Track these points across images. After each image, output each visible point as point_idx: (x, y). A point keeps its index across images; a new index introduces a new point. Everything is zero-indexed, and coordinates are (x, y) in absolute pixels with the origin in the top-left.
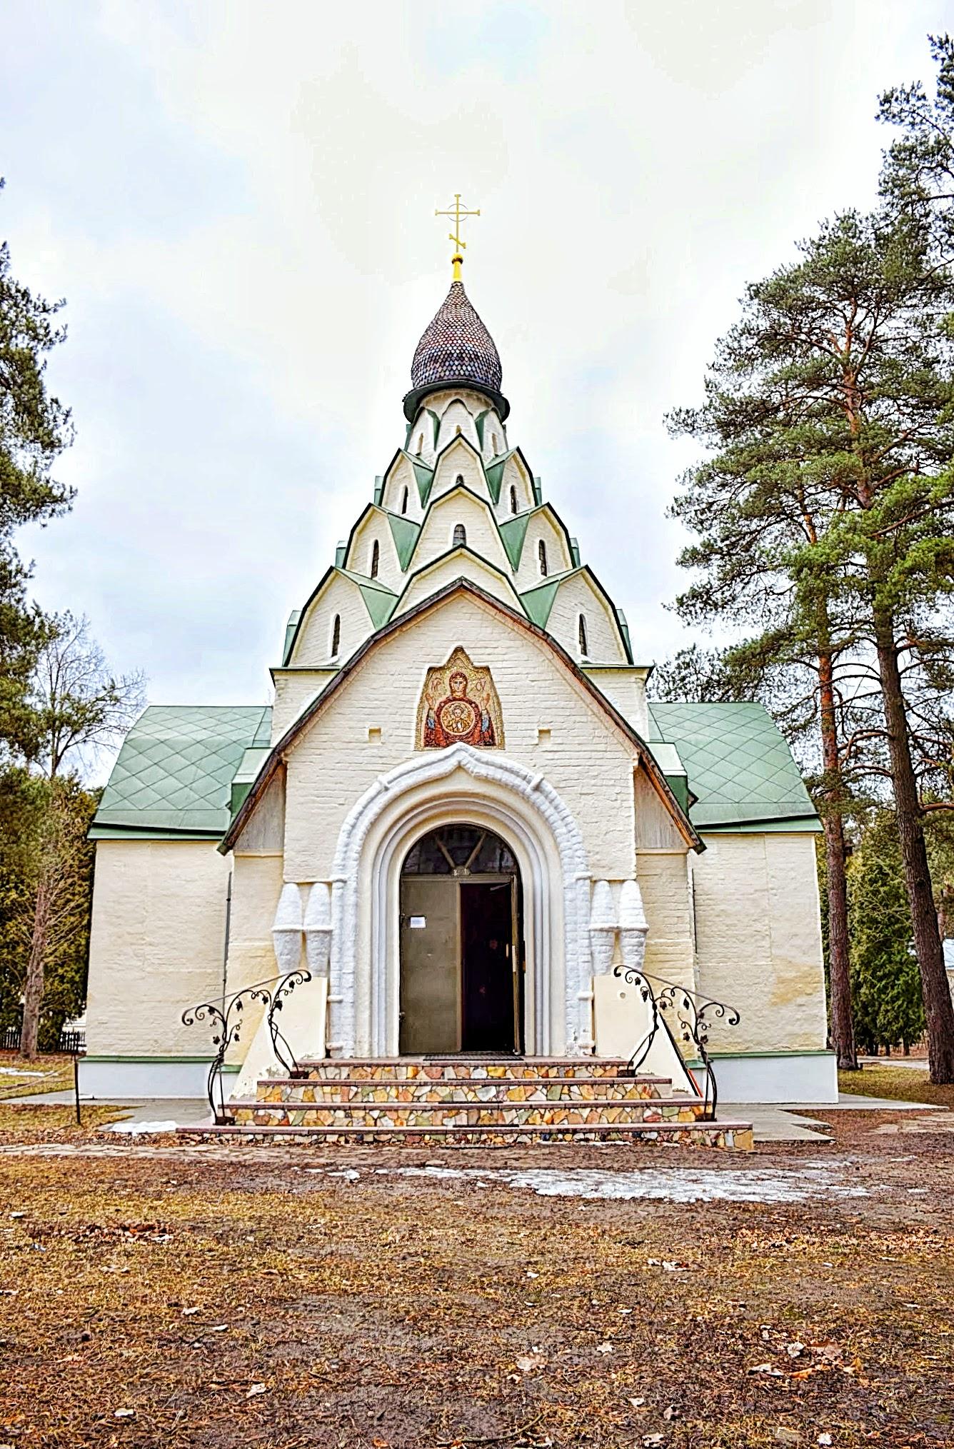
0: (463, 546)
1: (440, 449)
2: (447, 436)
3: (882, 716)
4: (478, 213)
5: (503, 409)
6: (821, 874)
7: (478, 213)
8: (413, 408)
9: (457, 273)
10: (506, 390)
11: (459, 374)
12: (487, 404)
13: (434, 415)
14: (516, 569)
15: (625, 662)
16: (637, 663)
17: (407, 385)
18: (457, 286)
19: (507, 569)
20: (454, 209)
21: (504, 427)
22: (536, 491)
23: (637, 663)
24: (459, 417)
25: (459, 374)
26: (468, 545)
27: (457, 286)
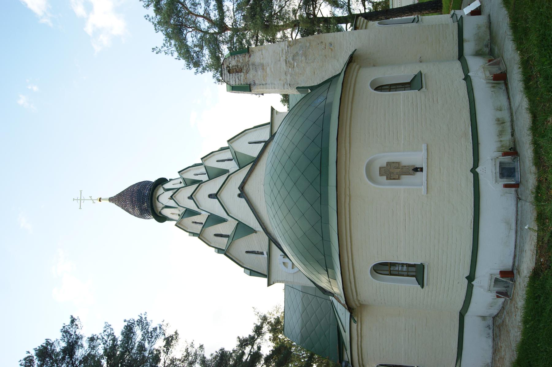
0: (216, 194)
1: (177, 206)
2: (172, 203)
3: (286, 32)
5: (162, 181)
8: (161, 218)
9: (105, 199)
10: (153, 179)
11: (143, 199)
13: (163, 208)
14: (228, 171)
16: (199, 233)
17: (153, 221)
18: (111, 200)
21: (171, 180)
22: (196, 165)
23: (199, 233)
24: (164, 198)
25: (143, 199)
26: (215, 192)
27: (111, 200)
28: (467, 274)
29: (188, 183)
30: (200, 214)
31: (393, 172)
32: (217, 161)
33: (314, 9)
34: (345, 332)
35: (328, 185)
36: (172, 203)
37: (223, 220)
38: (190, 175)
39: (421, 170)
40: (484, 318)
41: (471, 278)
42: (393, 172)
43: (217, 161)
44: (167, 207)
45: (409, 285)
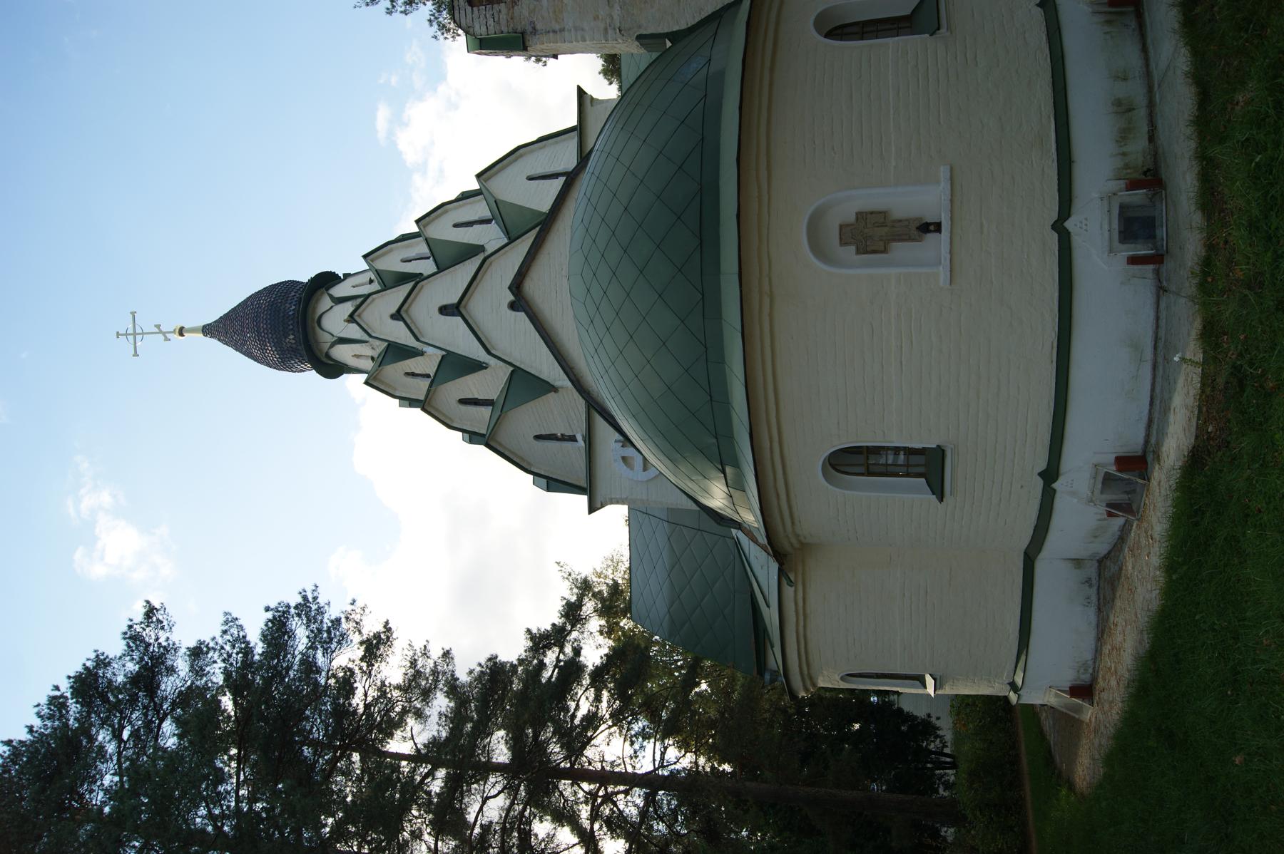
1: (366, 337)
2: (353, 331)
4: (136, 355)
5: (326, 280)
6: (952, 706)
7: (136, 355)
8: (332, 369)
9: (193, 330)
10: (304, 277)
12: (328, 356)
13: (333, 345)
14: (481, 249)
15: (575, 134)
18: (208, 330)
19: (481, 257)
20: (131, 338)
21: (347, 276)
27: (208, 330)
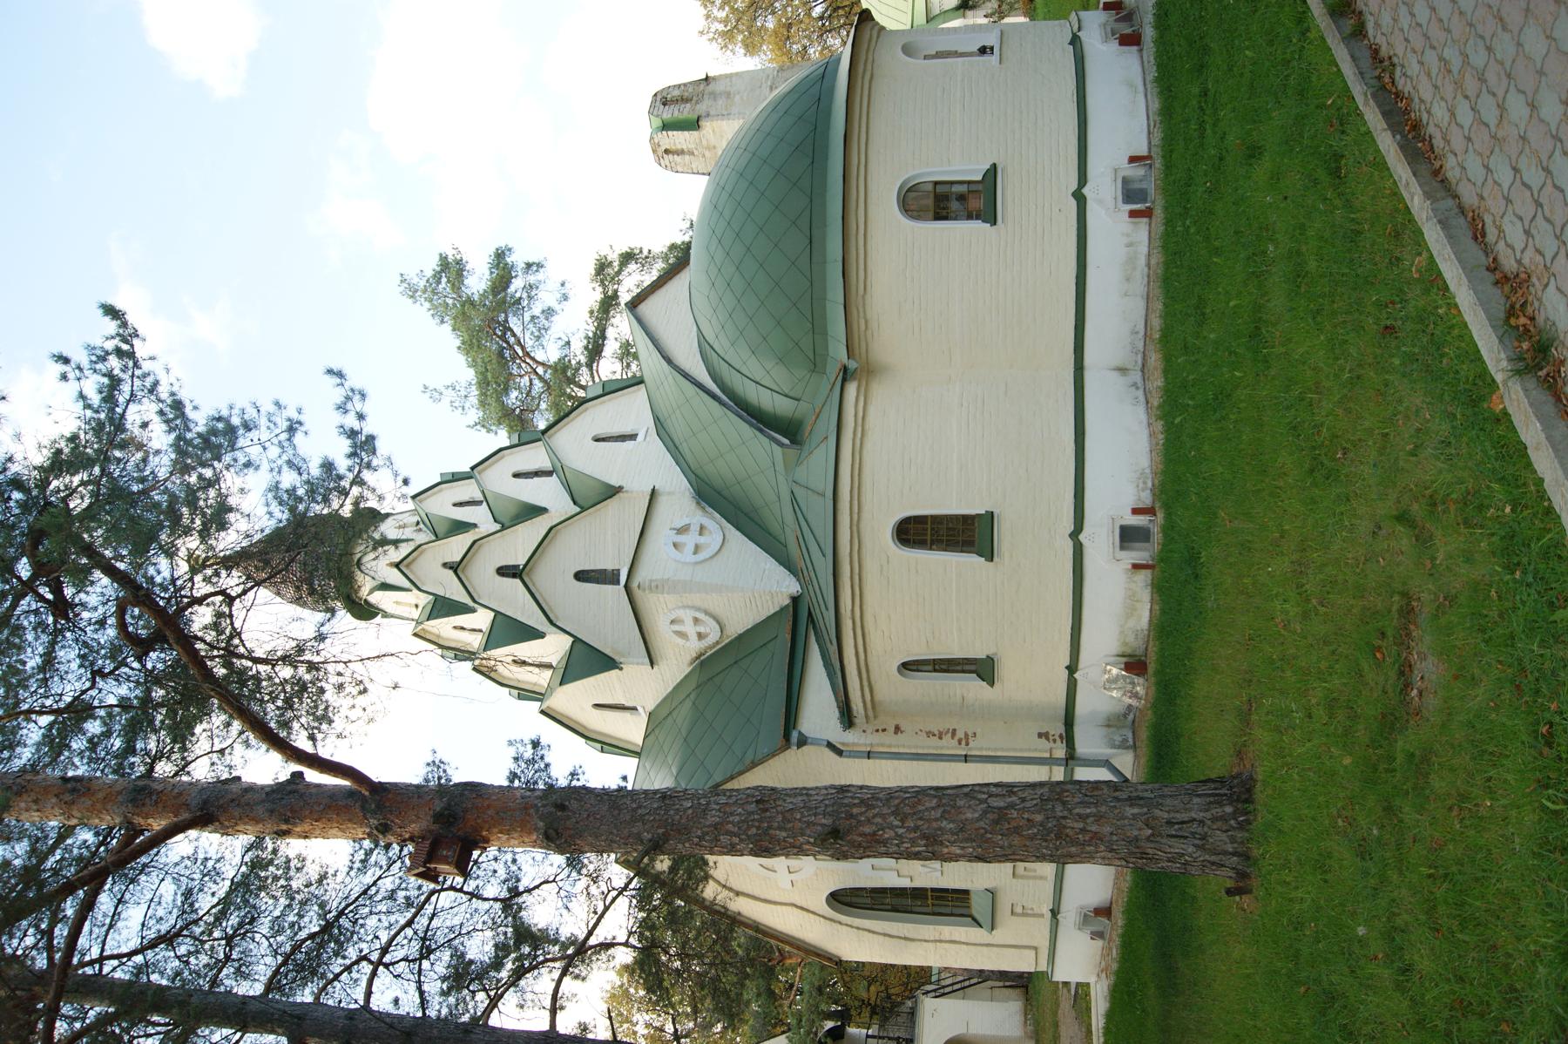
2: (395, 577)
14: (541, 511)
28: (1074, 186)
29: (441, 530)
30: (473, 611)
31: (941, 202)
32: (516, 475)
33: (555, 941)
34: (843, 900)
35: (825, 262)
36: (395, 577)
37: (537, 635)
38: (443, 506)
39: (992, 48)
40: (1104, 912)
41: (1072, 669)
42: (941, 202)
43: (516, 475)
44: (385, 587)
45: (969, 687)
